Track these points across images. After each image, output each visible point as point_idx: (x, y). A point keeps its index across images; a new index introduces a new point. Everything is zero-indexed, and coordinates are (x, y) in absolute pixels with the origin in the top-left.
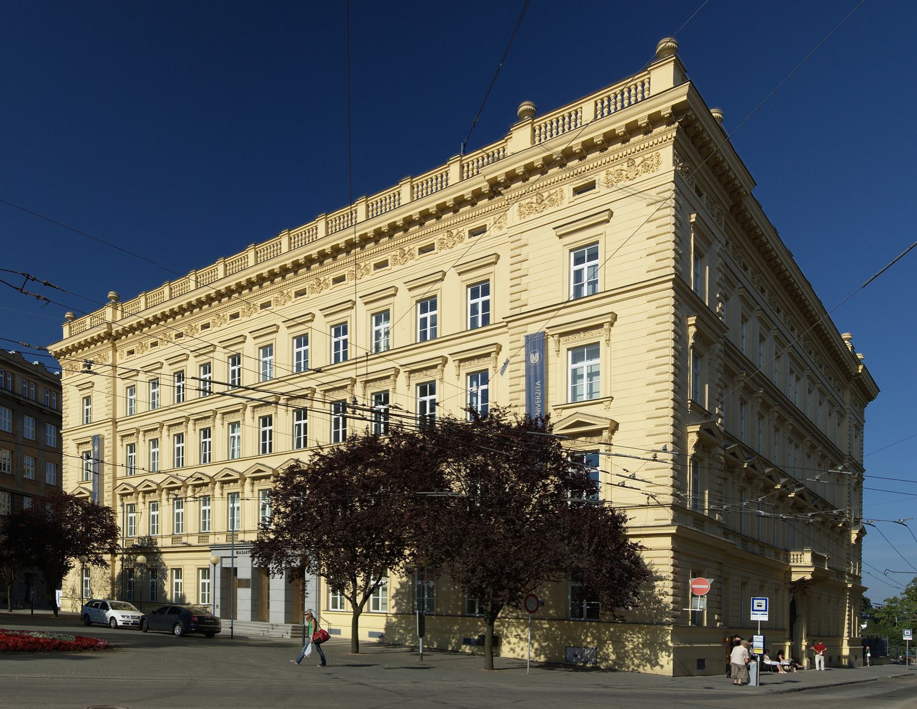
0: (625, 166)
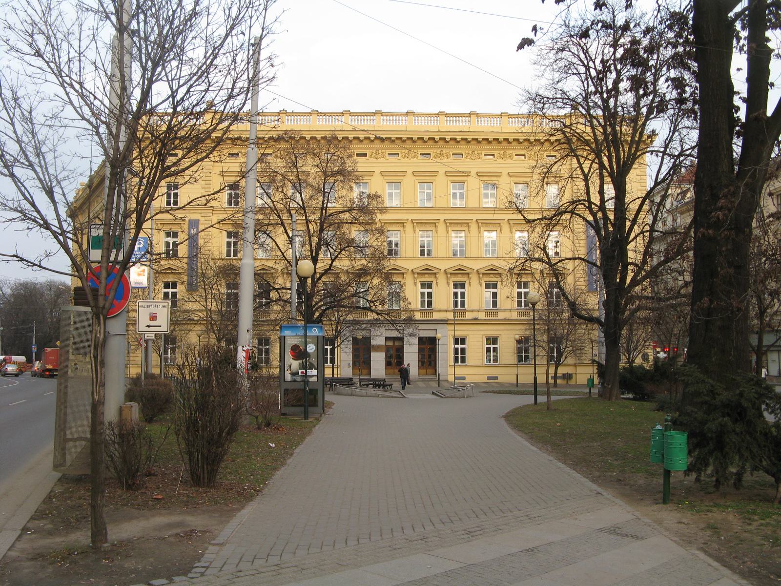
0: (470, 152)
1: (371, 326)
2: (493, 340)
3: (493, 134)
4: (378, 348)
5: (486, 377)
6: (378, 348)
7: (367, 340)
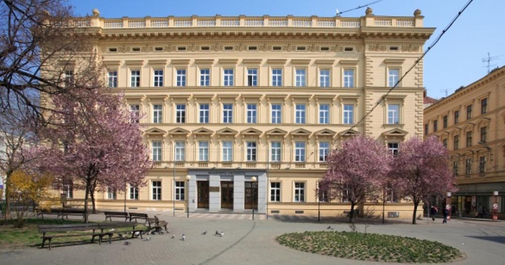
1: (209, 173)
2: (275, 185)
3: (142, 30)
4: (216, 189)
5: (294, 211)
6: (216, 189)
7: (207, 183)
